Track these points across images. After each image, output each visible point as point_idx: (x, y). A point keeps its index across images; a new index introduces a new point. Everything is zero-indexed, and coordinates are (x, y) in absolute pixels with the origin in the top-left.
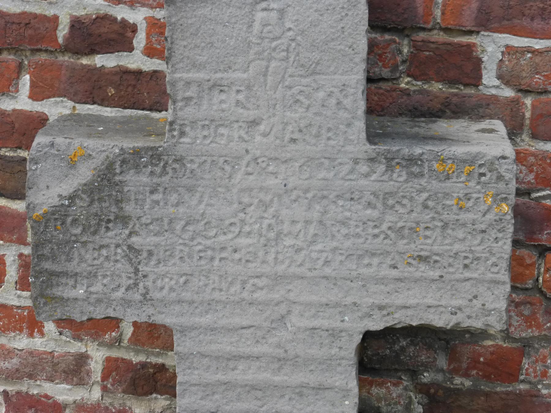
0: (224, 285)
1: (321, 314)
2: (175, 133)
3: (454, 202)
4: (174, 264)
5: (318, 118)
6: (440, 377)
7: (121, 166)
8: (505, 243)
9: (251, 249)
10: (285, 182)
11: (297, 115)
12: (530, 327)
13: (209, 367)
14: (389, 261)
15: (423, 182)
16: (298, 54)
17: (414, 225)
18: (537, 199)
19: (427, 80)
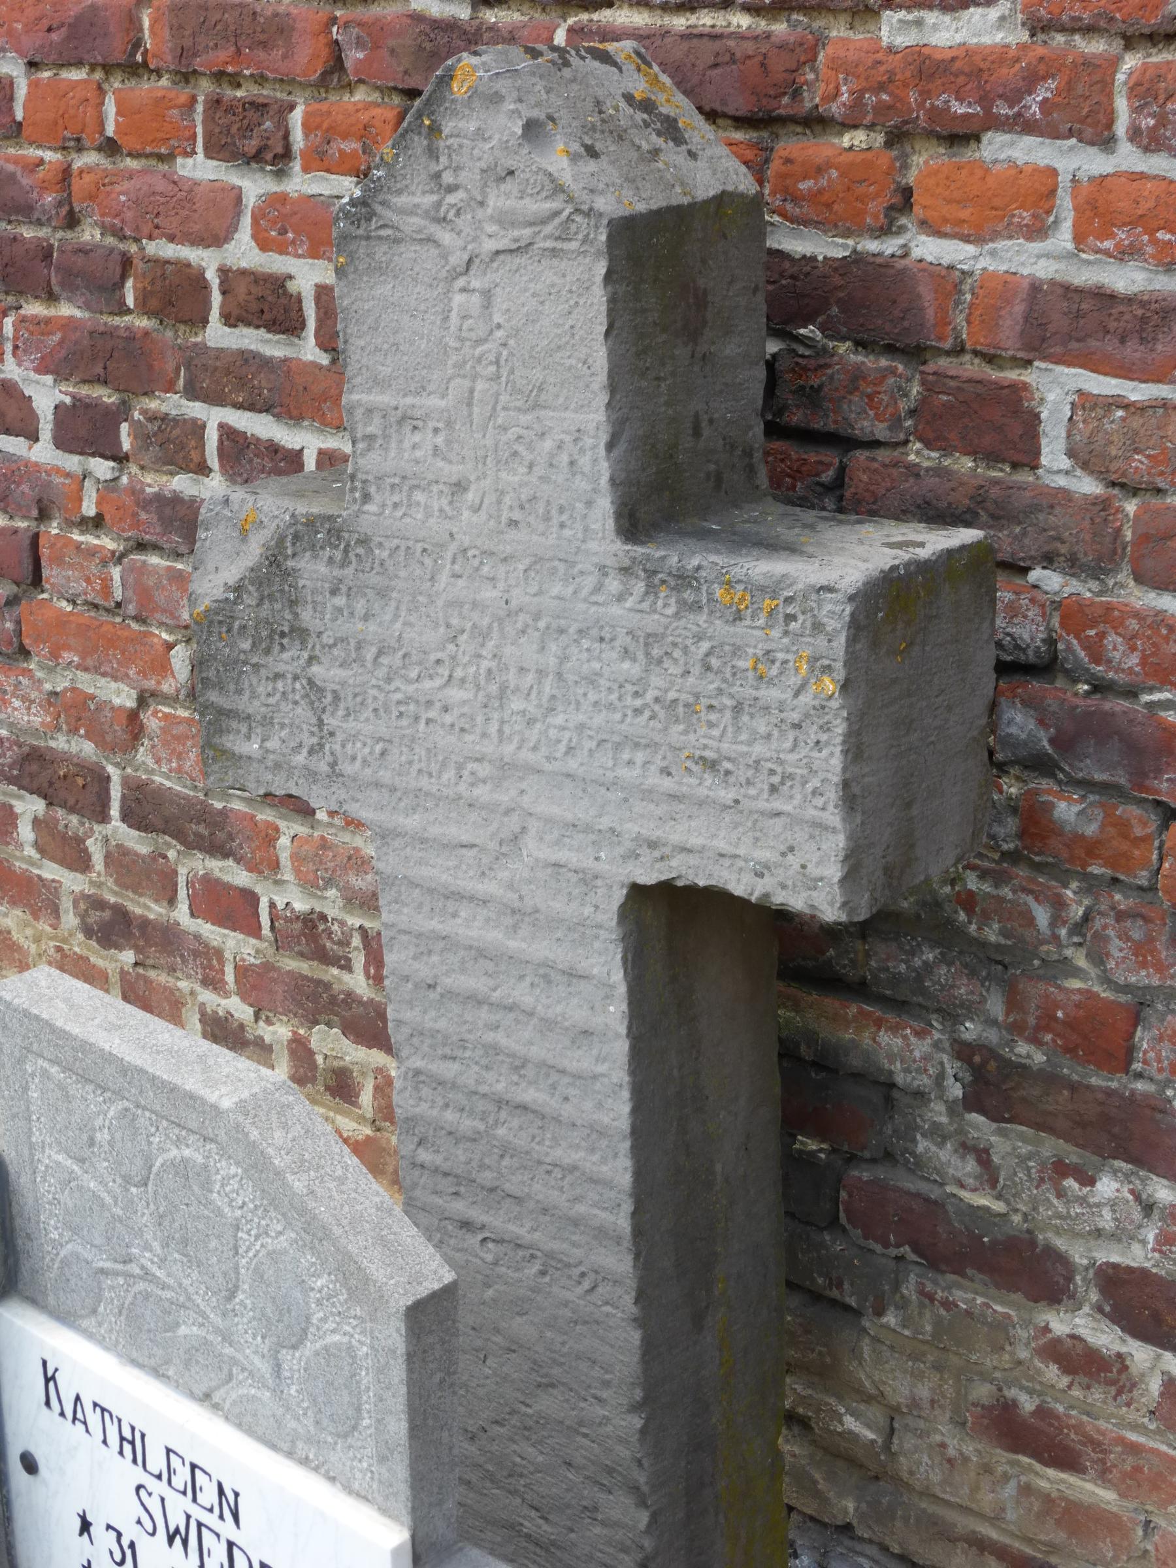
0: (434, 768)
1: (567, 840)
2: (357, 495)
3: (749, 664)
4: (367, 720)
5: (545, 487)
6: (992, 1036)
7: (294, 544)
8: (832, 754)
9: (465, 710)
10: (506, 596)
11: (517, 479)
12: (1144, 965)
13: (420, 905)
14: (659, 763)
15: (702, 619)
16: (512, 372)
17: (691, 700)
18: (1150, 705)
19: (946, 449)
